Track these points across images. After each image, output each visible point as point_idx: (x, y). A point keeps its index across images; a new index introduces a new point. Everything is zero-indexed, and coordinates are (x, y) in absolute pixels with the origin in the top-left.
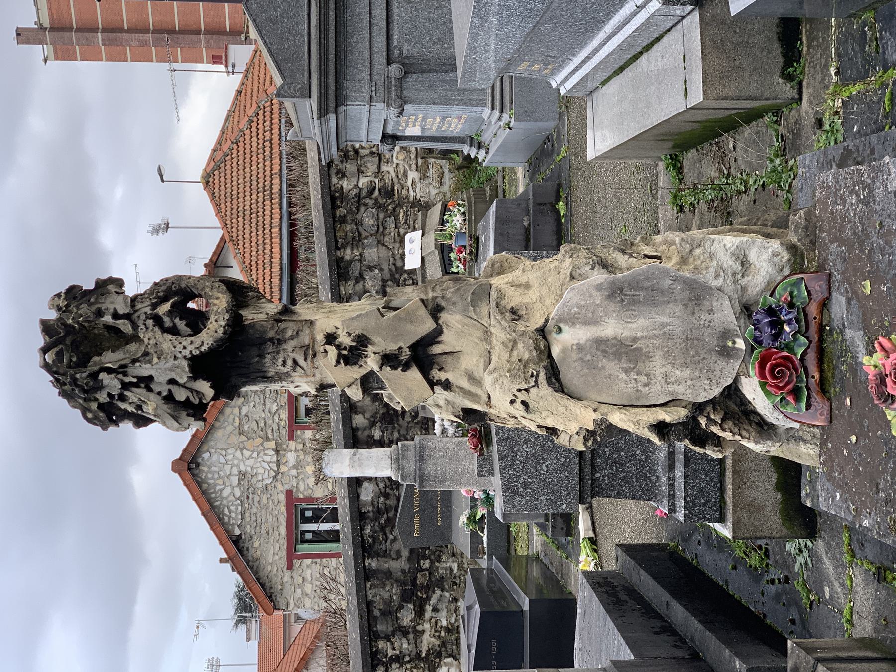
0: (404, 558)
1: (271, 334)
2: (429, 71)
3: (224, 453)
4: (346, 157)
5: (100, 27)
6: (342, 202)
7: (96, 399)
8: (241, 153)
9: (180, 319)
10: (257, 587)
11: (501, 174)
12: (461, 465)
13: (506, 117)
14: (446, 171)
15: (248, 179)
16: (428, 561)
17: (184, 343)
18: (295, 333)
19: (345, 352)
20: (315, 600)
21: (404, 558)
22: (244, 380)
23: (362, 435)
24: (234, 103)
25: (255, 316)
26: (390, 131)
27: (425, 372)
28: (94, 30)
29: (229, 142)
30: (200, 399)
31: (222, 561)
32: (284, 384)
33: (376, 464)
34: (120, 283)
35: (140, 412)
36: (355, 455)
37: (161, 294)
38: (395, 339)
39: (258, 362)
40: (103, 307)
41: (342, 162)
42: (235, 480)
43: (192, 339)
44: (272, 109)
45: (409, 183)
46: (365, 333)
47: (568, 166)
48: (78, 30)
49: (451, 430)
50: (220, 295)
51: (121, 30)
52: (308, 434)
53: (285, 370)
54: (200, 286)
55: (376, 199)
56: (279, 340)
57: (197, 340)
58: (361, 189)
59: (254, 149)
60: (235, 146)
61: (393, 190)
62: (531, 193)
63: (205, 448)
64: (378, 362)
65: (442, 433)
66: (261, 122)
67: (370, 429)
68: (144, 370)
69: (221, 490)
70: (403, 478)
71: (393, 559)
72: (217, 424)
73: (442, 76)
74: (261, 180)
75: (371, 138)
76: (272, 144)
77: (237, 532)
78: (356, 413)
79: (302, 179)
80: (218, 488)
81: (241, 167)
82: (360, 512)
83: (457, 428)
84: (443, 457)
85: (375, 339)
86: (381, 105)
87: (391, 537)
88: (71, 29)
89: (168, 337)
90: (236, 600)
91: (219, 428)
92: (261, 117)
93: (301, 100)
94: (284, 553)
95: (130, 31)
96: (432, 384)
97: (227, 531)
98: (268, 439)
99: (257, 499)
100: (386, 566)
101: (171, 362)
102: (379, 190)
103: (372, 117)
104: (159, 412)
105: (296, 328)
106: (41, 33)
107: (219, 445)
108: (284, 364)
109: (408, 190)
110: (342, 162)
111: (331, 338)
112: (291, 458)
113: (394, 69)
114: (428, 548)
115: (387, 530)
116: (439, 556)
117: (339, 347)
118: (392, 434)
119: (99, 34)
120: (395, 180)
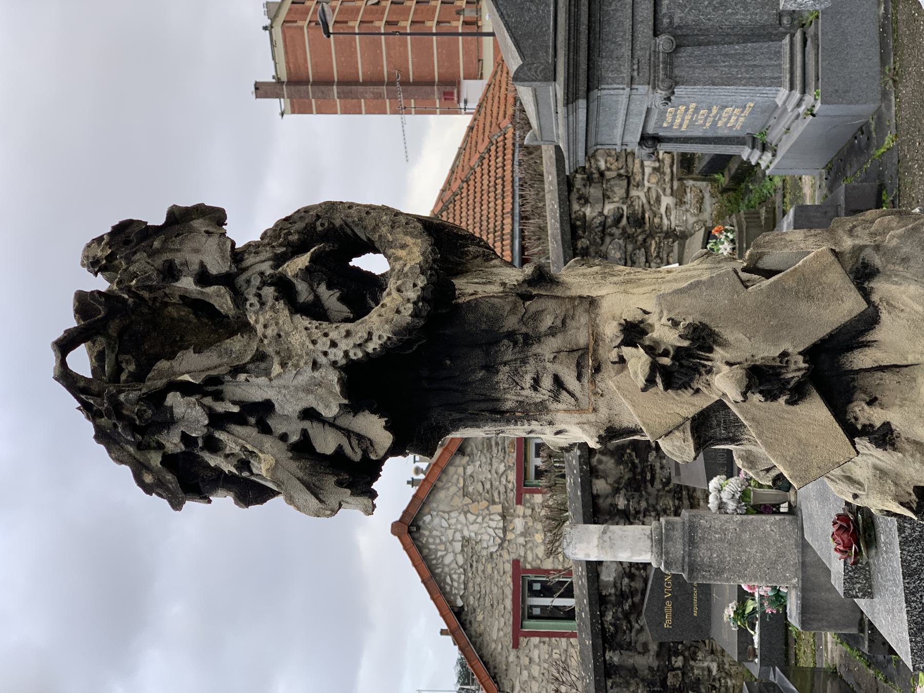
0: (652, 653)
1: (511, 323)
2: (708, 44)
3: (446, 516)
4: (589, 180)
5: (336, 80)
6: (584, 232)
7: (160, 446)
8: (471, 192)
9: (329, 287)
10: (480, 665)
11: (780, 192)
12: (745, 551)
13: (809, 99)
14: (707, 196)
15: (477, 219)
16: (681, 658)
17: (333, 335)
18: (559, 323)
19: (666, 361)
20: (544, 684)
21: (652, 653)
22: (456, 416)
23: (604, 503)
24: (464, 142)
25: (480, 289)
26: (651, 130)
27: (839, 408)
28: (330, 83)
29: (459, 181)
30: (365, 453)
31: (443, 632)
32: (535, 425)
33: (629, 545)
34: (217, 217)
35: (245, 474)
36: (604, 532)
37: (294, 238)
38: (773, 335)
39: (482, 380)
40: (178, 259)
41: (585, 186)
42: (458, 546)
43: (349, 326)
44: (505, 144)
45: (663, 210)
46: (706, 320)
47: (895, 161)
48: (315, 83)
49: (731, 506)
50: (409, 240)
51: (356, 83)
52: (538, 498)
53: (538, 397)
54: (370, 222)
55: (624, 229)
56: (526, 336)
57: (360, 329)
58: (606, 217)
59: (485, 187)
60: (465, 185)
61: (643, 218)
62: (842, 198)
63: (426, 510)
64: (739, 382)
65: (719, 508)
66: (493, 158)
67: (614, 496)
68: (255, 389)
69: (443, 557)
70: (668, 565)
71: (639, 653)
72: (440, 484)
73: (725, 48)
74: (492, 220)
75: (627, 139)
76: (504, 181)
77: (460, 603)
78: (597, 477)
79: (539, 212)
80: (439, 554)
81: (471, 207)
82: (600, 594)
83: (739, 503)
84: (721, 540)
85: (729, 334)
86: (643, 89)
87: (637, 626)
88: (306, 82)
89: (303, 321)
90: (459, 668)
91: (442, 488)
92: (493, 153)
93: (544, 84)
94: (509, 629)
95: (366, 83)
96: (852, 431)
97: (449, 602)
98: (494, 503)
99: (481, 568)
100: (631, 661)
101: (308, 373)
102: (628, 218)
103: (632, 107)
104: (281, 475)
105: (560, 312)
106: (278, 86)
107: (442, 507)
108: (536, 384)
109: (661, 218)
110: (585, 186)
111: (633, 332)
112: (519, 524)
113: (663, 42)
114: (682, 643)
115: (632, 618)
116: (695, 653)
117: (650, 350)
118: (639, 503)
119: (335, 87)
120: (647, 207)
